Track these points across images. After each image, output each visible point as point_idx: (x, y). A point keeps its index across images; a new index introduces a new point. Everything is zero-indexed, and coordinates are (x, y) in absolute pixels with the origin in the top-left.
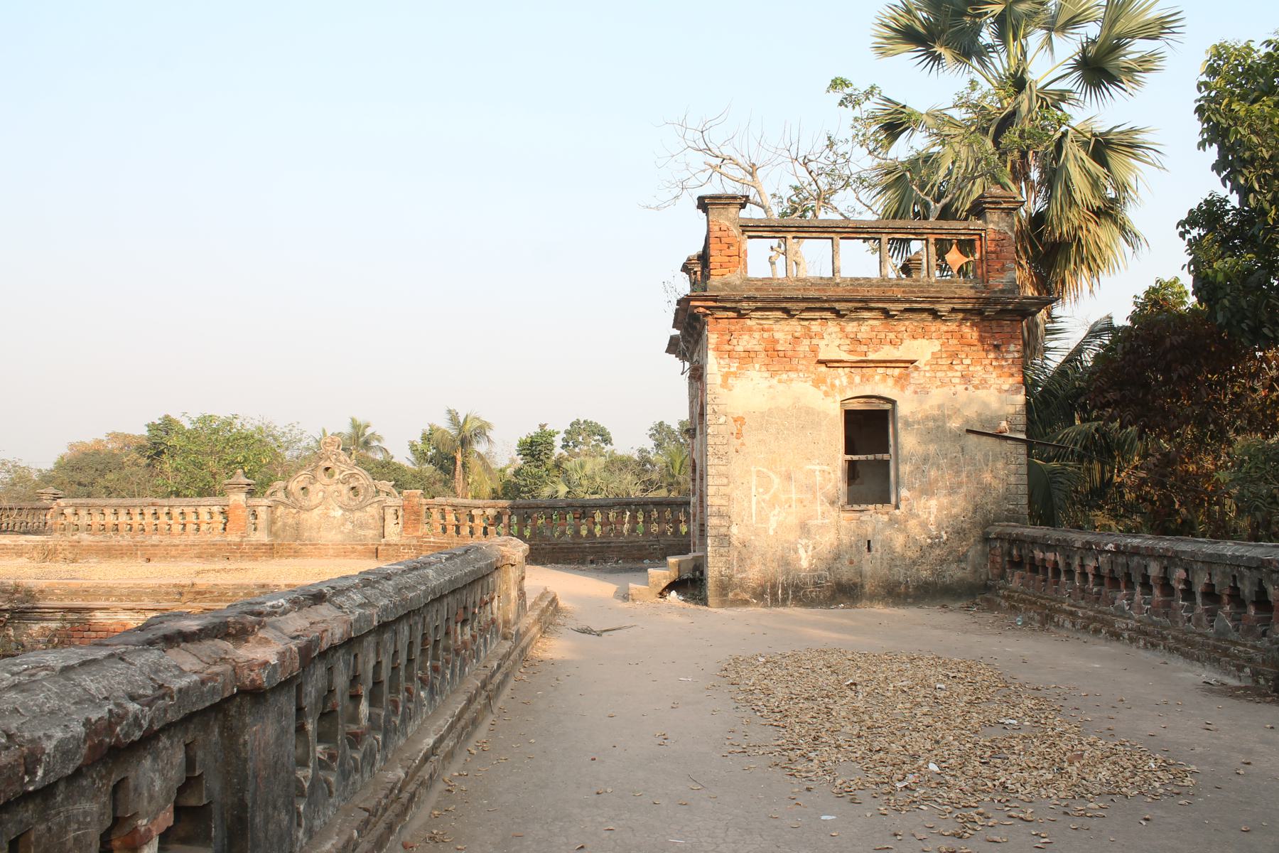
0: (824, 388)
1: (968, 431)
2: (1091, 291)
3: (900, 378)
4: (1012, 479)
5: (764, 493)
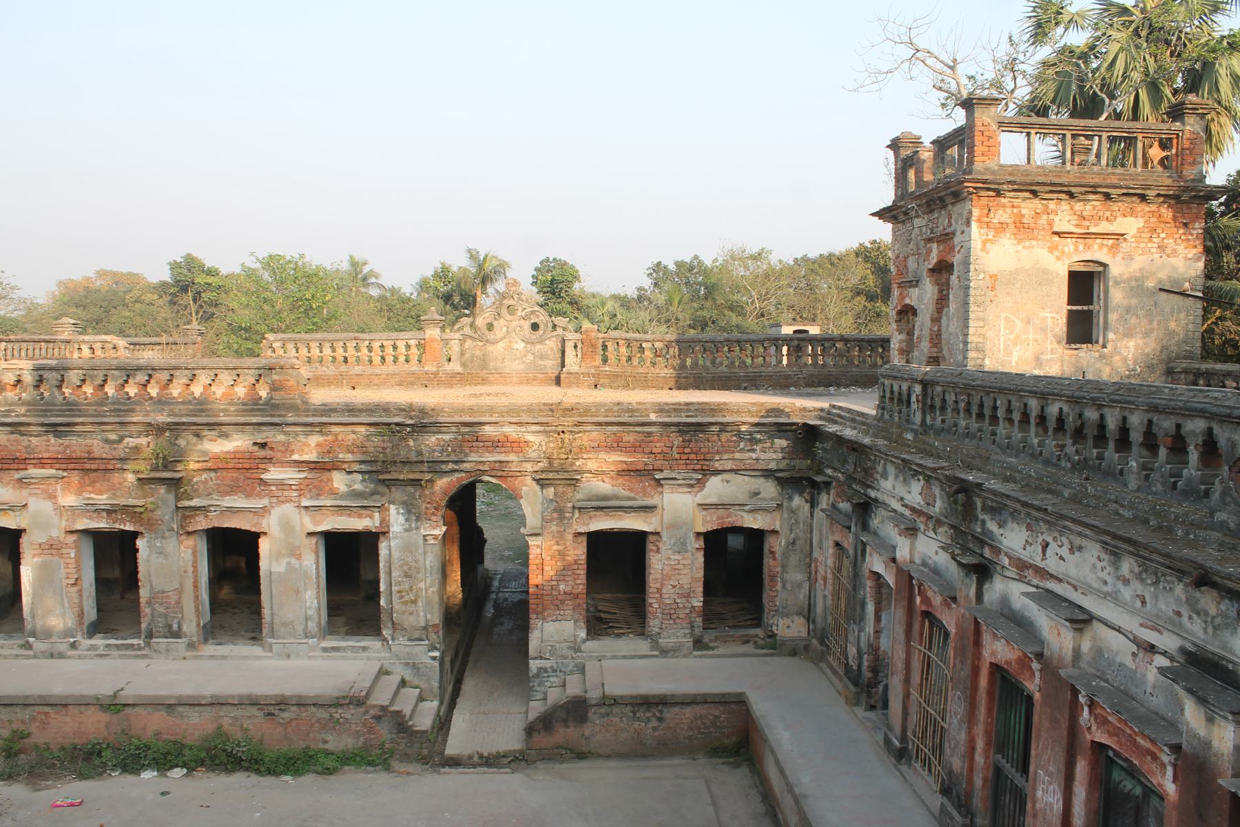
0: (1056, 253)
4: (1191, 327)
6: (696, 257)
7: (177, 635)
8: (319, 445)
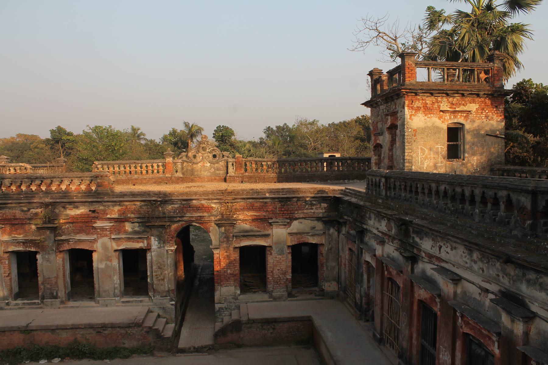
6: (285, 124)
7: (56, 297)
8: (119, 210)
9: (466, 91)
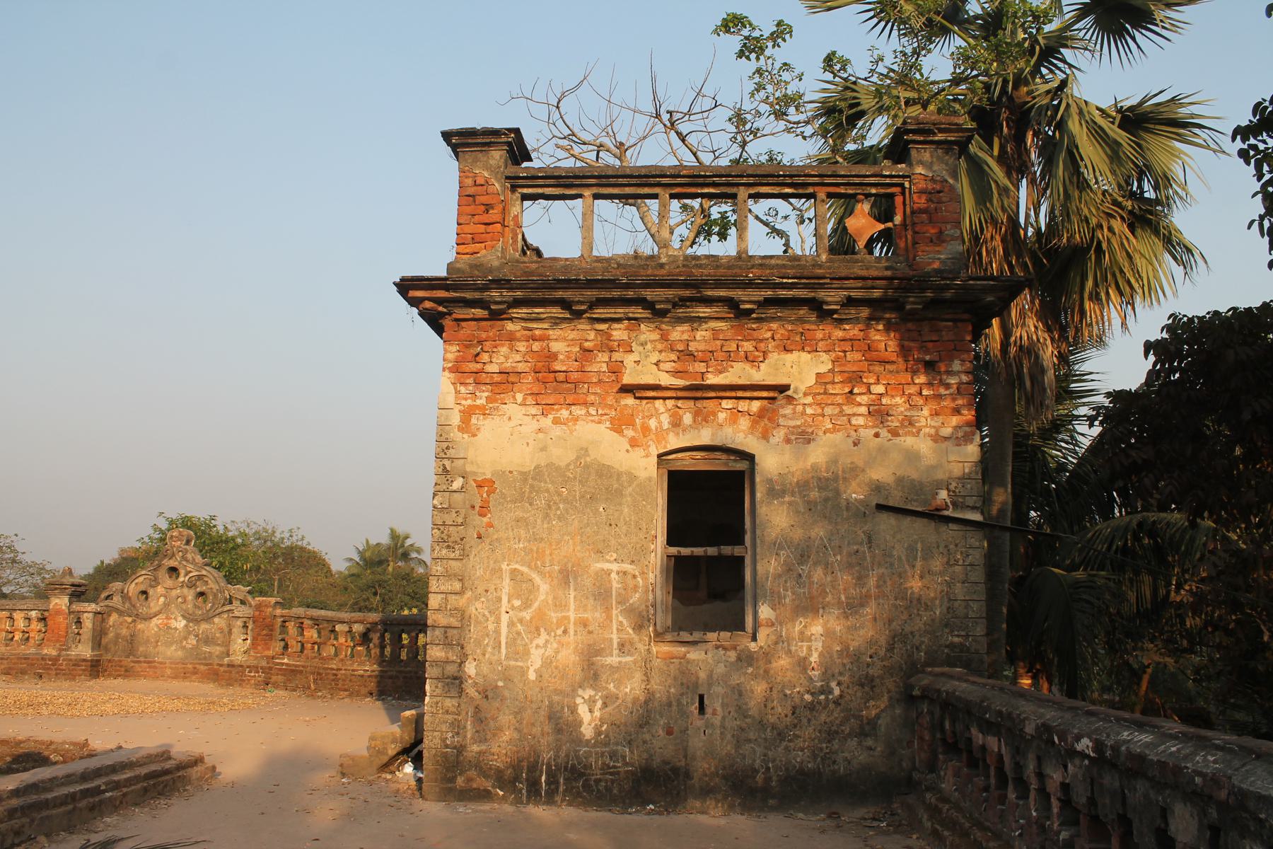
0: (630, 433)
1: (880, 507)
2: (1124, 324)
3: (761, 414)
5: (520, 609)
9: (749, 284)
